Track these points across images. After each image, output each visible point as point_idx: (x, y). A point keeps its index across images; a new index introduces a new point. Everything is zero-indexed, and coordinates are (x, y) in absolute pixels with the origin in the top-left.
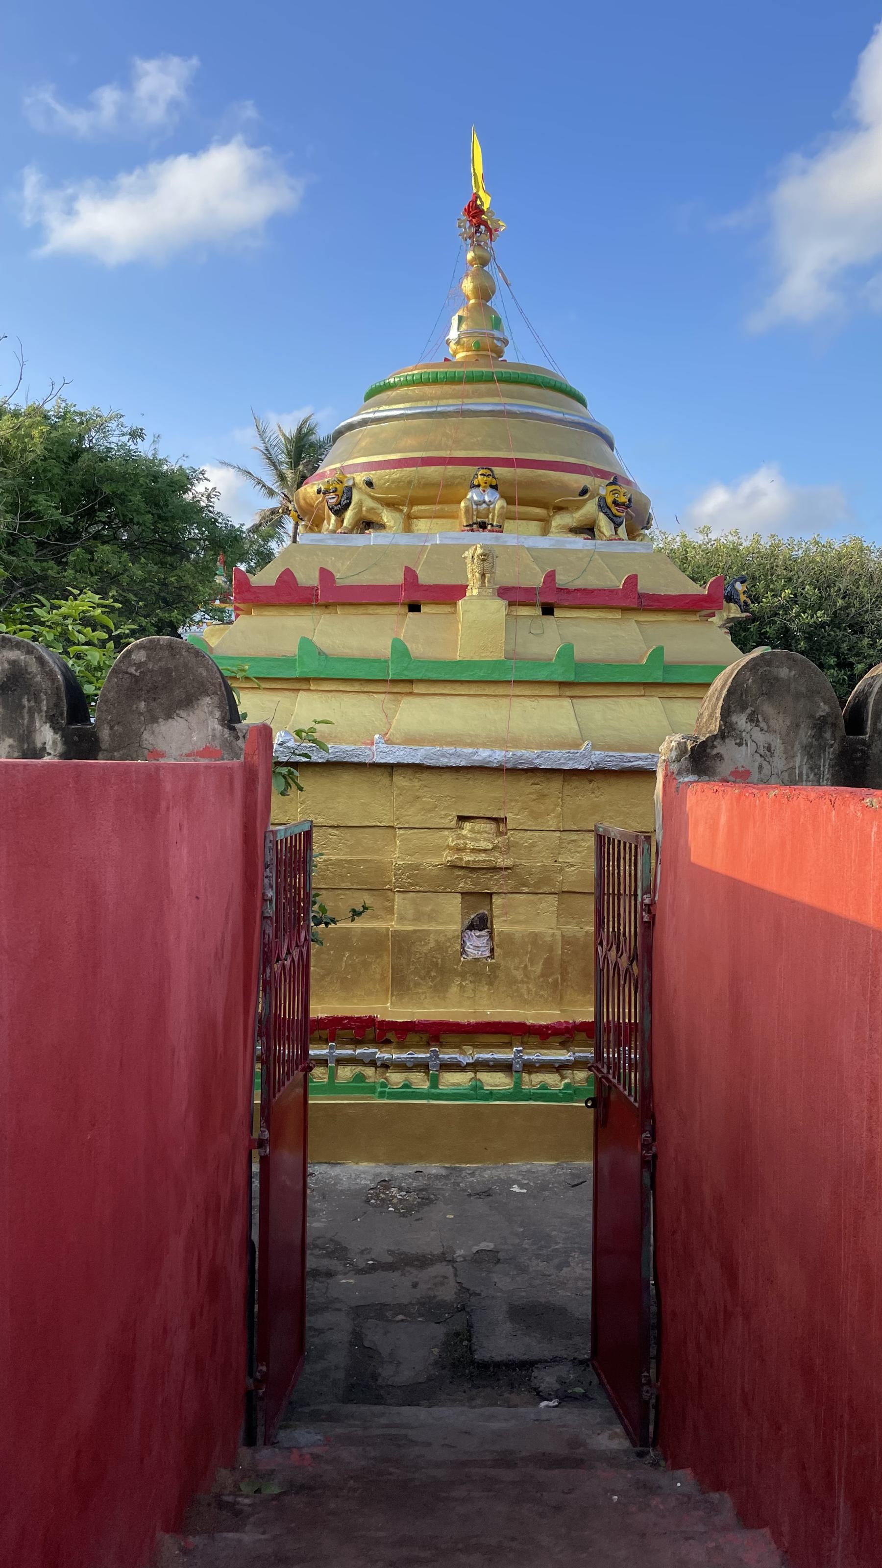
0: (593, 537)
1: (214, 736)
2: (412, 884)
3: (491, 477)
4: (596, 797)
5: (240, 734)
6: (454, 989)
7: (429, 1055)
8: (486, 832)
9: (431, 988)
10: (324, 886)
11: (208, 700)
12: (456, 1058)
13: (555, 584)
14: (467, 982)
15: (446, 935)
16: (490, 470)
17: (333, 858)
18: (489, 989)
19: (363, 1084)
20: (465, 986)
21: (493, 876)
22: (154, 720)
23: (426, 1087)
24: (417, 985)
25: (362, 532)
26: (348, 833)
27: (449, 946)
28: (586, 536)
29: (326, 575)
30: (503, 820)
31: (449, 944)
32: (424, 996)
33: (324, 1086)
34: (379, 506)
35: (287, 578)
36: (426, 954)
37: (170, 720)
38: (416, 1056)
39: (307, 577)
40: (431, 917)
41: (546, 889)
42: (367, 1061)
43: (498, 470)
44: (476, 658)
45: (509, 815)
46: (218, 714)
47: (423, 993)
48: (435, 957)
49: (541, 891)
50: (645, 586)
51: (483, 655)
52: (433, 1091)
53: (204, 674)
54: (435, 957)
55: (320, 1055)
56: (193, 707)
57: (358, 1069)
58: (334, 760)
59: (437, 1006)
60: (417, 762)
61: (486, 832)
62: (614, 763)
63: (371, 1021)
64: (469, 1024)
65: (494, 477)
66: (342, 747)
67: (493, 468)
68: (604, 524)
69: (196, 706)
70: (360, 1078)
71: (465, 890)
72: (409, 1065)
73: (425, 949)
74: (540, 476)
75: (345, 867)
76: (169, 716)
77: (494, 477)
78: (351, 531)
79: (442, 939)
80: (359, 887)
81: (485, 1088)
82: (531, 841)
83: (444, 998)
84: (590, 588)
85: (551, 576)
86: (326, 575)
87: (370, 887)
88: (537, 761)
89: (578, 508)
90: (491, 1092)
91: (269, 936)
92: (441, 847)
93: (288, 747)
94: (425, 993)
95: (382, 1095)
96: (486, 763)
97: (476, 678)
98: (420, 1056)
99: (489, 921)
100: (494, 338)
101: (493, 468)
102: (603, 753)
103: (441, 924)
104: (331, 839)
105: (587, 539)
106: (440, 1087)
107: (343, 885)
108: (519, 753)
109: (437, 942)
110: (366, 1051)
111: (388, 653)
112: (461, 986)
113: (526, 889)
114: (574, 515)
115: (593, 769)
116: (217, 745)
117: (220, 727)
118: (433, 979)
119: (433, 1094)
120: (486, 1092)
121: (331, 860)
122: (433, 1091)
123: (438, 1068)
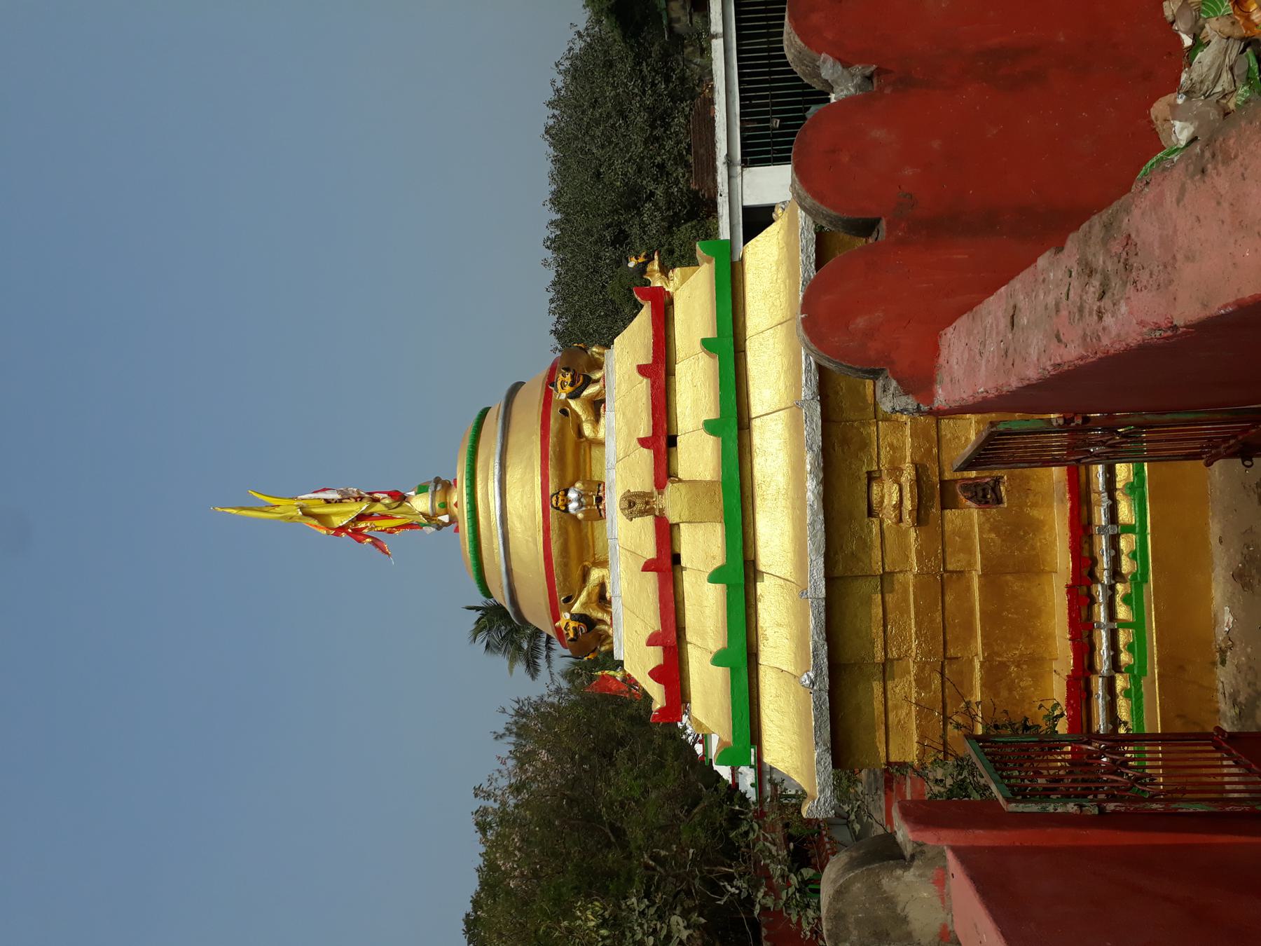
0: (603, 401)
1: (920, 876)
2: (936, 556)
3: (559, 496)
4: (842, 390)
5: (918, 849)
6: (1035, 513)
7: (1103, 536)
8: (882, 490)
9: (1034, 534)
10: (941, 637)
11: (885, 881)
12: (1105, 509)
13: (649, 438)
14: (1028, 501)
15: (983, 523)
16: (552, 496)
17: (914, 630)
18: (1034, 479)
19: (1133, 595)
20: (1032, 503)
21: (924, 481)
22: (909, 935)
23: (1134, 536)
24: (1033, 548)
25: (610, 602)
26: (890, 616)
27: (994, 519)
28: (602, 410)
29: (651, 642)
30: (869, 473)
31: (992, 520)
32: (1043, 541)
33: (1136, 631)
34: (586, 589)
35: (656, 674)
36: (1003, 541)
37: (908, 919)
38: (1104, 547)
39: (655, 657)
40: (967, 537)
41: (934, 433)
42: (1110, 593)
43: (552, 490)
44: (721, 506)
45: (864, 470)
46: (899, 872)
47: (1041, 542)
48: (1006, 532)
49: (935, 436)
50: (646, 358)
51: (718, 500)
52: (1137, 530)
53: (859, 885)
54: (1006, 532)
55: (1106, 636)
56: (893, 897)
57: (1118, 599)
58: (824, 634)
59: (1052, 528)
60: (823, 559)
61: (882, 490)
62: (813, 378)
63: (1071, 590)
64: (1071, 499)
65: (558, 493)
66: (811, 627)
67: (550, 493)
68: (591, 390)
69: (892, 894)
70: (1127, 600)
71: (939, 507)
72: (1113, 553)
73: (998, 541)
74: (554, 453)
75: (922, 619)
76: (904, 920)
77: (558, 493)
78: (610, 613)
79: (987, 526)
80: (940, 604)
81: (1132, 480)
82: (888, 449)
83: (1042, 522)
84: (651, 406)
85: (643, 442)
86: (651, 642)
87: (940, 594)
88: (815, 448)
89: (578, 416)
90: (1136, 474)
91: (1117, 806)
92: (898, 531)
93: (816, 676)
94: (1040, 539)
95: (1145, 579)
96: (820, 496)
97: (739, 505)
98: (1104, 544)
99: (966, 482)
100: (435, 490)
101: (550, 493)
102: (803, 389)
103: (972, 526)
104: (896, 632)
105: (605, 407)
106: (1134, 522)
107: (939, 619)
108: (808, 467)
109: (991, 530)
110: (1101, 594)
111: (719, 586)
112: (1031, 507)
113: (935, 450)
114: (584, 420)
115: (819, 397)
116: (931, 873)
117: (912, 869)
118: (1026, 533)
119: (1140, 530)
120: (1136, 479)
121: (916, 631)
122: (1137, 530)
123: (1115, 526)
